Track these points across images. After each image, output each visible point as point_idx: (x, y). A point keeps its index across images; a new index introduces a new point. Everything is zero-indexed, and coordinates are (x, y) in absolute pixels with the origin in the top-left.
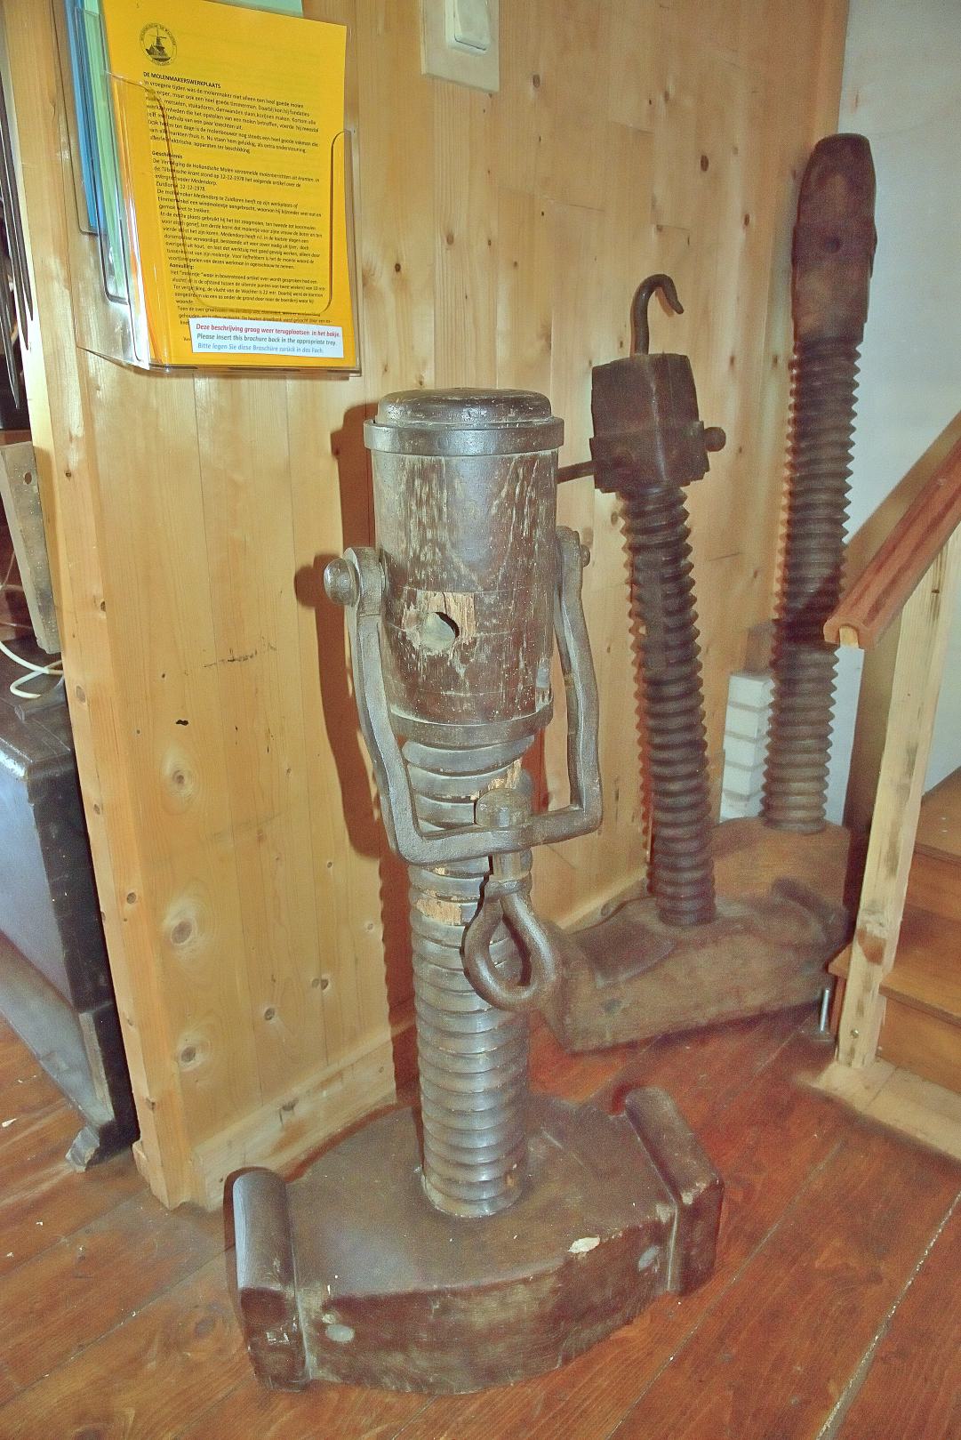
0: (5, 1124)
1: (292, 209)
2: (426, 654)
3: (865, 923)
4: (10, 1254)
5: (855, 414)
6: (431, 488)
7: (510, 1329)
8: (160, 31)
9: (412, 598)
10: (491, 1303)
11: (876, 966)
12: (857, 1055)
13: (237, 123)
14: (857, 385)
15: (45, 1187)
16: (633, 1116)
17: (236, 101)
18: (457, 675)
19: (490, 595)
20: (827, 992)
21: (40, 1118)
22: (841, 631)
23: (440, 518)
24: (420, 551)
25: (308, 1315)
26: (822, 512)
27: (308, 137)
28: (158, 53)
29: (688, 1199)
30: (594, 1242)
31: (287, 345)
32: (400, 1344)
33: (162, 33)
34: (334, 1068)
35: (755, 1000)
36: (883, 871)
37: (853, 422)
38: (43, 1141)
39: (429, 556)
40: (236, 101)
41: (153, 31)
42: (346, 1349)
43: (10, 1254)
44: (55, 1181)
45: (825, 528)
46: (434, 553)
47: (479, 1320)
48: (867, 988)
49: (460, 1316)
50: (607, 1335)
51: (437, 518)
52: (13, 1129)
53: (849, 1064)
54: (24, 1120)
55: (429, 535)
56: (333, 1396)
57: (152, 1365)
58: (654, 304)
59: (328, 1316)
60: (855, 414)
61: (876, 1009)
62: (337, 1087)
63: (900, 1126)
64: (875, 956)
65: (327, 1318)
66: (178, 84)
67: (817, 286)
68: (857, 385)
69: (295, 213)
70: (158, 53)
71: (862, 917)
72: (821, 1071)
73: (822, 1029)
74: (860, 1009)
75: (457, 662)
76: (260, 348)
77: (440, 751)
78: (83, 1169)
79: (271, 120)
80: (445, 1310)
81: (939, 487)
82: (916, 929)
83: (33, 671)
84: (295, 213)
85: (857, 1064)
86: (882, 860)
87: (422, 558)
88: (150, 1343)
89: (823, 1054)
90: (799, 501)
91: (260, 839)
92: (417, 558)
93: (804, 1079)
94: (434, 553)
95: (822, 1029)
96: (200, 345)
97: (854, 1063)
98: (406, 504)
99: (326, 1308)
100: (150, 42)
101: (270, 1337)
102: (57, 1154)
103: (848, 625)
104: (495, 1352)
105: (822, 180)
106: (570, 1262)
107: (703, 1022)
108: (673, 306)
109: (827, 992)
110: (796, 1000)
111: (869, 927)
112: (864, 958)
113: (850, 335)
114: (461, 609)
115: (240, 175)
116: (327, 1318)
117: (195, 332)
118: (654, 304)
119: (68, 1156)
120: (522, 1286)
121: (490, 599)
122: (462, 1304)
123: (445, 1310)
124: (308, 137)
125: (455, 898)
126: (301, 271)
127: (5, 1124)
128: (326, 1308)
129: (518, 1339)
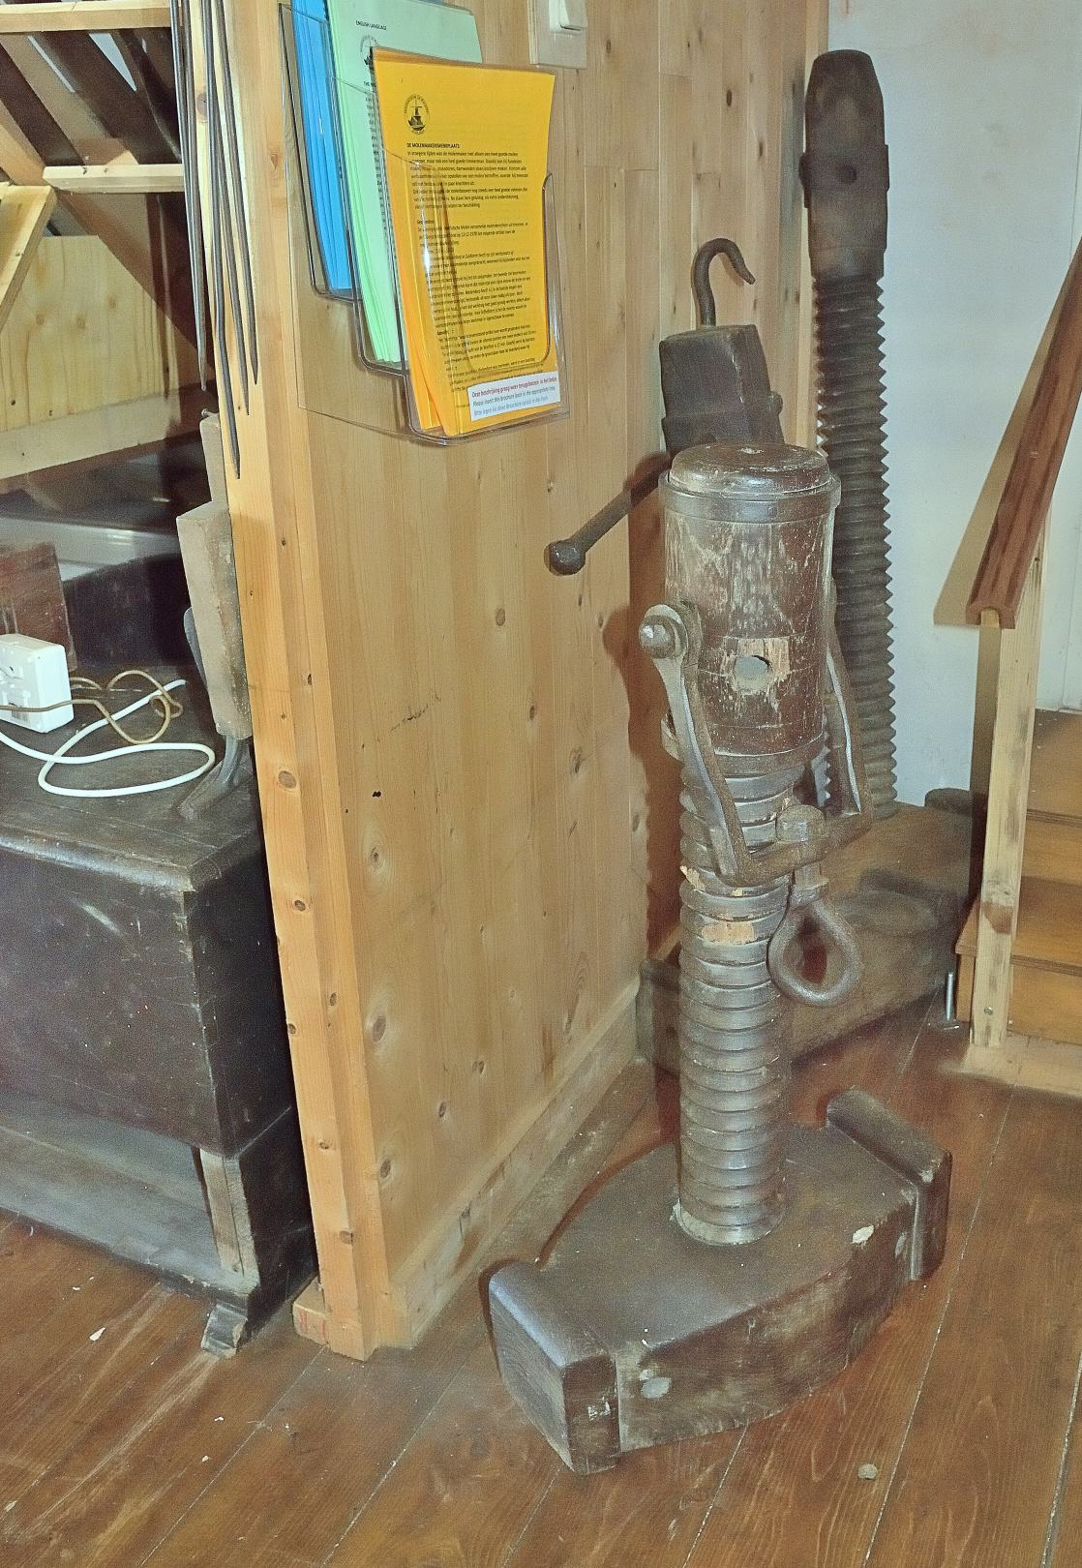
0: (95, 1337)
1: (509, 256)
2: (744, 694)
3: (989, 894)
4: (206, 1458)
5: (883, 356)
6: (757, 550)
7: (811, 1333)
8: (418, 101)
9: (732, 647)
10: (797, 1309)
11: (1004, 936)
12: (993, 1033)
13: (470, 180)
14: (882, 323)
15: (198, 1383)
16: (840, 1122)
17: (470, 158)
18: (772, 709)
19: (801, 636)
20: (951, 976)
21: (133, 1320)
22: (983, 613)
23: (765, 574)
24: (743, 605)
25: (624, 1378)
26: (863, 466)
27: (520, 183)
28: (416, 123)
29: (927, 1177)
30: (869, 1231)
31: (527, 398)
32: (715, 1381)
33: (420, 104)
34: (492, 1164)
35: (880, 1000)
36: (1005, 839)
37: (882, 364)
38: (157, 1342)
39: (752, 608)
40: (470, 158)
41: (412, 103)
42: (661, 1404)
43: (206, 1458)
44: (204, 1375)
45: (868, 483)
46: (757, 606)
47: (788, 1330)
48: (997, 961)
49: (774, 1330)
50: (876, 1327)
51: (761, 574)
52: (108, 1342)
53: (987, 1044)
54: (115, 1327)
55: (753, 590)
56: (650, 1460)
57: (447, 1498)
58: (717, 264)
59: (645, 1371)
60: (883, 356)
61: (1005, 976)
62: (500, 1184)
63: (1052, 1089)
64: (1002, 927)
65: (644, 1375)
66: (430, 149)
67: (835, 218)
68: (882, 323)
69: (512, 260)
70: (416, 123)
71: (986, 889)
72: (962, 1056)
73: (948, 1017)
74: (993, 984)
75: (773, 698)
76: (512, 406)
77: (738, 780)
78: (232, 1352)
79: (494, 172)
80: (760, 1328)
81: (1032, 460)
82: (1031, 891)
83: (64, 755)
84: (512, 260)
85: (994, 1042)
86: (1003, 826)
87: (745, 610)
88: (430, 1482)
89: (957, 1040)
90: (839, 455)
91: (433, 910)
92: (739, 610)
93: (948, 1067)
94: (757, 606)
95: (948, 1017)
96: (476, 413)
97: (991, 1042)
98: (730, 564)
99: (643, 1364)
100: (411, 113)
101: (592, 1411)
102: (185, 1348)
103: (991, 608)
104: (800, 1361)
105: (830, 103)
106: (856, 1250)
107: (835, 1034)
108: (739, 271)
109: (951, 976)
110: (917, 993)
111: (994, 898)
112: (992, 931)
113: (871, 268)
114: (777, 651)
115: (474, 230)
116: (644, 1375)
117: (472, 400)
118: (717, 264)
119: (204, 1343)
120: (822, 1285)
121: (800, 640)
122: (774, 1316)
123: (760, 1328)
124: (520, 183)
125: (752, 916)
126: (519, 318)
127: (95, 1337)
128: (643, 1364)
129: (817, 1343)
